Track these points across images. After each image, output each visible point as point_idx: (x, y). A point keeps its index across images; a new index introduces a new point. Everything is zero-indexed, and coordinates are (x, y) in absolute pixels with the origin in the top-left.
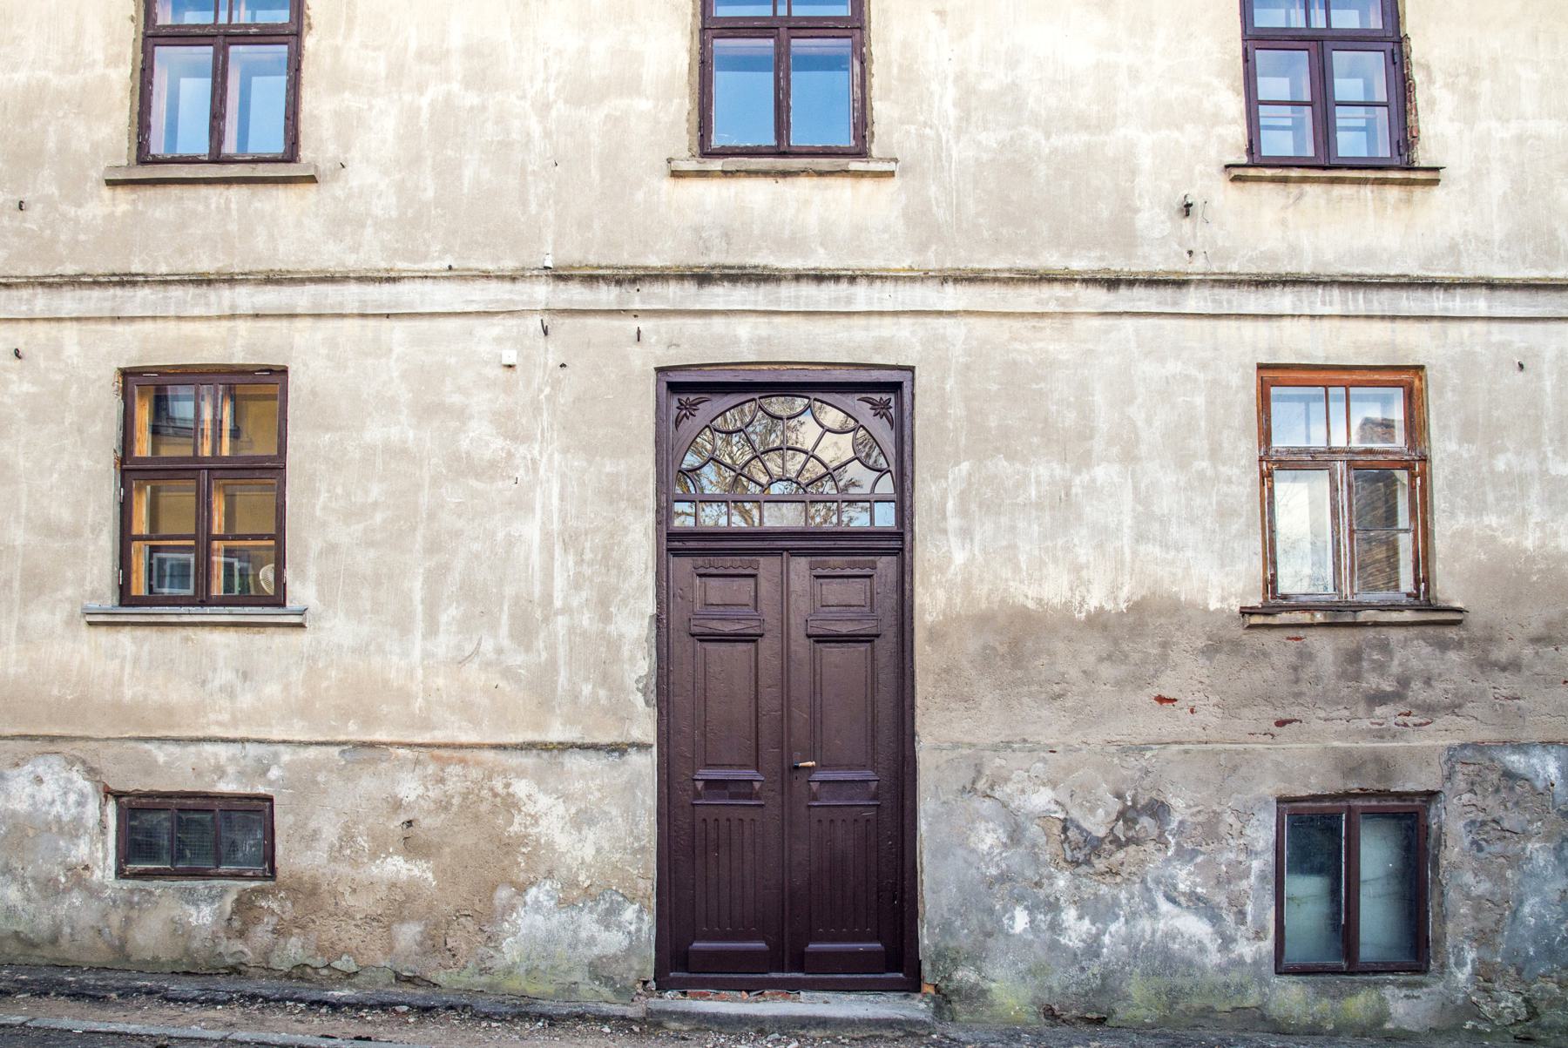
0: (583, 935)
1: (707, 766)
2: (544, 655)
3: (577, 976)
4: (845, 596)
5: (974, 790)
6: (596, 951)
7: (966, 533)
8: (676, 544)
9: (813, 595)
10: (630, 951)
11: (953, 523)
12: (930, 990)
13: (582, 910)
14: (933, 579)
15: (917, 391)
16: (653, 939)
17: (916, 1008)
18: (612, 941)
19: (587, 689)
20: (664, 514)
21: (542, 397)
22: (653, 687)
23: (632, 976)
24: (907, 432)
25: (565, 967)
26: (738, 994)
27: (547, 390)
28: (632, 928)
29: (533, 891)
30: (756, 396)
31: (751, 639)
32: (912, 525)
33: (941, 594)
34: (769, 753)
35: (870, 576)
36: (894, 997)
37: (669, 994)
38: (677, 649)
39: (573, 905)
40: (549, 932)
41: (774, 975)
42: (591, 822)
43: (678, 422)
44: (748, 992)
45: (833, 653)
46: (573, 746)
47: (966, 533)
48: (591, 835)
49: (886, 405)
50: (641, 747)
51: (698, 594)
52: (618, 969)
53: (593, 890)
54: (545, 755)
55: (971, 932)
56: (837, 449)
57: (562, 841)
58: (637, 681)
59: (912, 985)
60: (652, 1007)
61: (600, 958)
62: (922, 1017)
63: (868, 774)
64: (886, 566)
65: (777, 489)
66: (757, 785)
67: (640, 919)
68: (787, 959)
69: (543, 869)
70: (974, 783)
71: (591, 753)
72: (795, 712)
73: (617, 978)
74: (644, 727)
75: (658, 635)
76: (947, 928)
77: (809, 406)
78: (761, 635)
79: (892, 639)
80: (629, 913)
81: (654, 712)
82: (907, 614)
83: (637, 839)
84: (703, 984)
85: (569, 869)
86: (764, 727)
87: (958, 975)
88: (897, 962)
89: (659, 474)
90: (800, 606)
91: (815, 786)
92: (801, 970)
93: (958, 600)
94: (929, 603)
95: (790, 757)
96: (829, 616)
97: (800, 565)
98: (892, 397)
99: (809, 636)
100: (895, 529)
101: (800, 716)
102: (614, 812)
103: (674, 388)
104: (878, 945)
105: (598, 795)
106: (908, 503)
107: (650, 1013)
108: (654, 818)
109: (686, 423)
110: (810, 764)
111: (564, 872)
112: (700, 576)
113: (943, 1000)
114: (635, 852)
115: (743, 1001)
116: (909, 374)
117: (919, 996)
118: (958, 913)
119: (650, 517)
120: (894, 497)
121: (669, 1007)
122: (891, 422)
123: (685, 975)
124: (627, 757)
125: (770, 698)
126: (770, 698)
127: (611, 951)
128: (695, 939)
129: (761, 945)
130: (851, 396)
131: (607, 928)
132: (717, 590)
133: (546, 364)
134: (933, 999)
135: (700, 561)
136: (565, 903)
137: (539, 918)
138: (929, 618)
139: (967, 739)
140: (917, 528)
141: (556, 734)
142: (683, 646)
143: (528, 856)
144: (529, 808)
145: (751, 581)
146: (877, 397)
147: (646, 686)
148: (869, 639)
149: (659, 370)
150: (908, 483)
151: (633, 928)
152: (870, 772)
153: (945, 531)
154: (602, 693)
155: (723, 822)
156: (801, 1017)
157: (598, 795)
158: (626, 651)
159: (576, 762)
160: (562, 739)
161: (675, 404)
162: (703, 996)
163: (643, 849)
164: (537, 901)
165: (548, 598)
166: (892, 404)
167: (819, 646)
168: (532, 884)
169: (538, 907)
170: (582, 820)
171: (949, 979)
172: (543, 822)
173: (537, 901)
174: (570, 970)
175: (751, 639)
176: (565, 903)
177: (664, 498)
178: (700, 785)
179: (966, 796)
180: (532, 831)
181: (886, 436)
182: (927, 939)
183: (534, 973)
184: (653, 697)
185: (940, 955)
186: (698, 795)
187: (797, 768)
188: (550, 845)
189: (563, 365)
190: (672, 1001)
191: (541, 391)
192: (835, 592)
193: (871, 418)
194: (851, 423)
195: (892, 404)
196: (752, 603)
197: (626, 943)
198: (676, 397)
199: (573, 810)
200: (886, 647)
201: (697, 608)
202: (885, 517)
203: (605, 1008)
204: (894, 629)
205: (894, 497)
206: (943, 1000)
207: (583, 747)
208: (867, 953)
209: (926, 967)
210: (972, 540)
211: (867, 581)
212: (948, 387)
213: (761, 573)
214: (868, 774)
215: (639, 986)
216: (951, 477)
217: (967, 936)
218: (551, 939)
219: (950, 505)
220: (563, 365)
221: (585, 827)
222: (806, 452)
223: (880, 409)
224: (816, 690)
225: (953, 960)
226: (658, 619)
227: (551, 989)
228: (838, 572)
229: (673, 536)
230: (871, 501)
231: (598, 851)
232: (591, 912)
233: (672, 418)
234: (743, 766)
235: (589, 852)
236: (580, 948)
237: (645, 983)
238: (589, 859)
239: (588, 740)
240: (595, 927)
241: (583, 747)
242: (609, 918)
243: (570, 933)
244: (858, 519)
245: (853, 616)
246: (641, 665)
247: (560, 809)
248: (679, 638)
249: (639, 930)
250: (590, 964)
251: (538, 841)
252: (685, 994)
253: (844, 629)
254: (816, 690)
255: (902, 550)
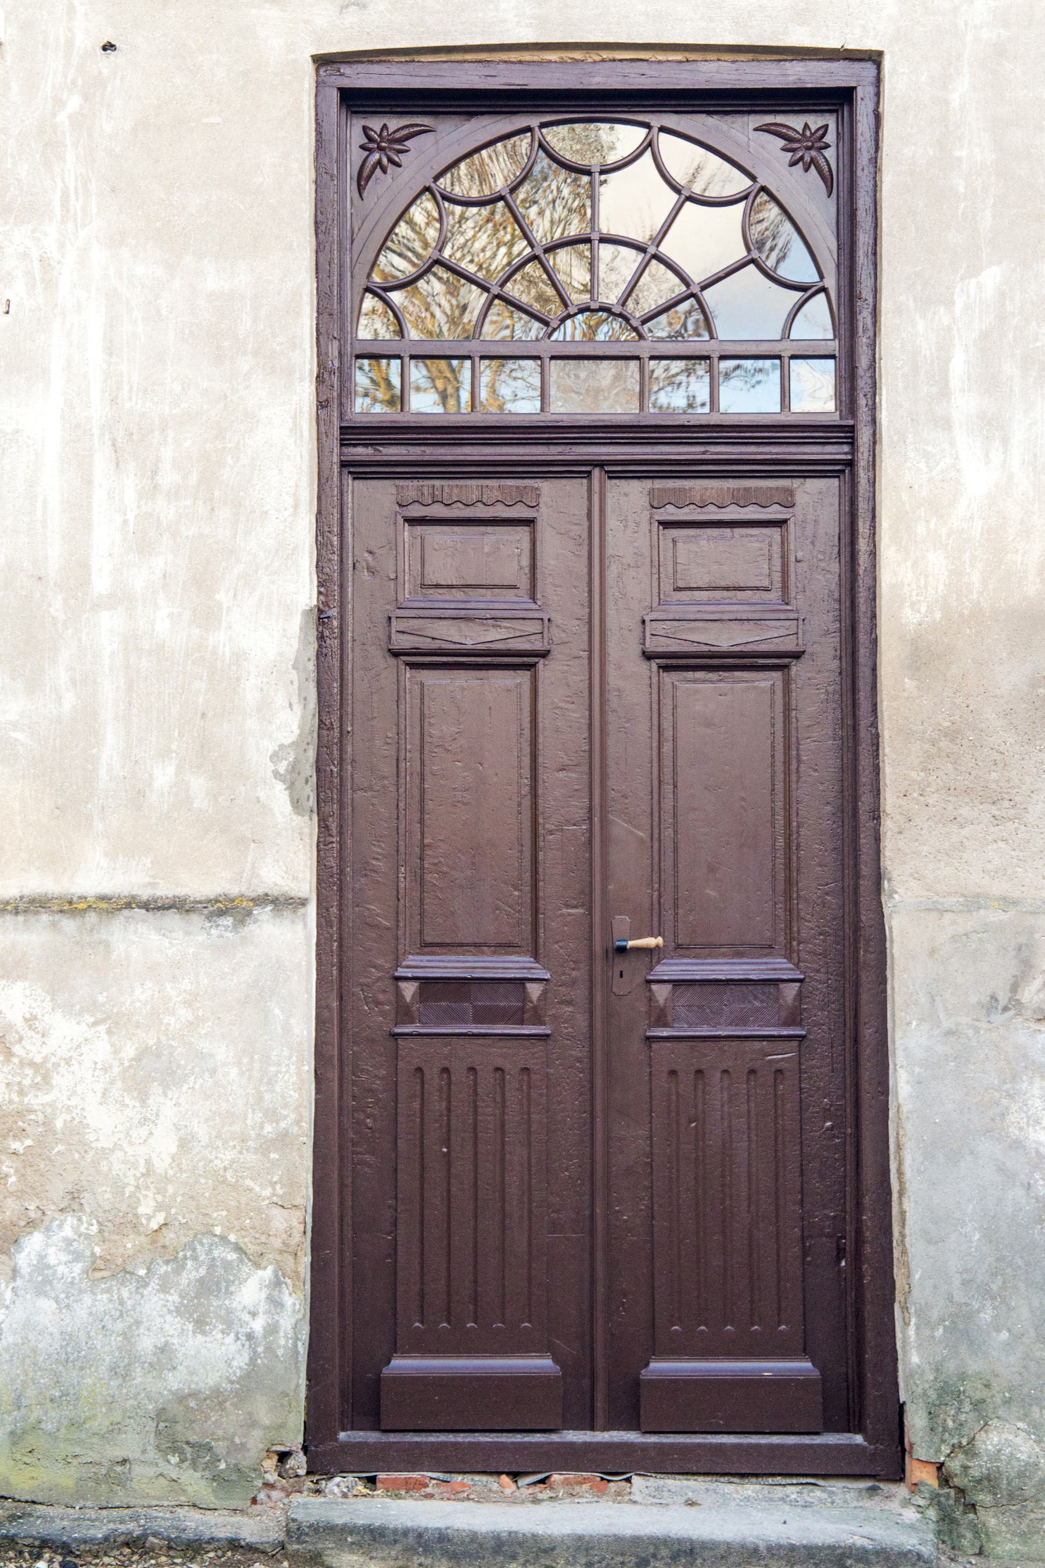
0: (146, 1343)
1: (427, 947)
2: (69, 700)
3: (129, 1445)
4: (724, 570)
5: (1013, 1005)
6: (174, 1381)
7: (992, 427)
8: (362, 451)
9: (657, 567)
10: (250, 1382)
11: (964, 404)
12: (928, 1478)
13: (143, 1283)
14: (921, 529)
15: (888, 108)
16: (303, 1349)
17: (896, 1518)
18: (211, 1357)
19: (163, 775)
20: (332, 384)
21: (62, 117)
22: (309, 770)
23: (255, 1442)
24: (863, 201)
25: (100, 1422)
26: (491, 1481)
27: (74, 103)
28: (260, 1319)
29: (34, 1242)
30: (534, 121)
31: (525, 661)
32: (873, 408)
33: (937, 563)
34: (562, 916)
35: (781, 523)
36: (843, 1492)
37: (336, 1485)
38: (359, 684)
39: (124, 1273)
40: (68, 1337)
41: (573, 1436)
42: (170, 1078)
43: (362, 180)
44: (515, 1475)
45: (701, 694)
46: (130, 903)
47: (992, 427)
48: (167, 1107)
49: (817, 141)
50: (283, 904)
51: (409, 564)
52: (222, 1426)
53: (169, 1237)
54: (69, 925)
55: (1017, 1337)
56: (707, 240)
57: (103, 1123)
58: (275, 757)
59: (885, 1461)
60: (300, 1515)
61: (181, 1398)
62: (910, 1542)
63: (777, 966)
64: (816, 500)
65: (573, 330)
66: (534, 990)
67: (275, 1303)
68: (605, 1404)
69: (57, 1190)
70: (1015, 988)
71: (172, 919)
72: (619, 827)
73: (220, 1447)
74: (288, 857)
75: (321, 655)
76: (961, 1328)
77: (649, 145)
78: (544, 654)
79: (837, 659)
80: (251, 1290)
81: (308, 827)
82: (863, 606)
83: (272, 1116)
84: (414, 1459)
85: (119, 1189)
86: (551, 753)
87: (991, 1441)
88: (848, 1409)
89: (323, 296)
90: (630, 590)
91: (661, 993)
92: (634, 1424)
93: (975, 578)
94: (913, 580)
95: (608, 927)
96: (691, 612)
97: (629, 498)
98: (830, 120)
99: (648, 656)
100: (835, 419)
101: (628, 833)
102: (222, 1053)
103: (355, 101)
104: (803, 1366)
105: (185, 1014)
106: (863, 362)
107: (295, 1531)
108: (309, 1066)
109: (381, 184)
110: (651, 942)
111: (105, 1195)
112: (412, 521)
113: (958, 1501)
114: (265, 1147)
115: (503, 1499)
116: (869, 69)
117: (901, 1490)
118: (987, 1294)
119: (306, 393)
120: (834, 347)
121: (339, 1516)
122: (828, 180)
123: (373, 1437)
124: (251, 928)
125: (563, 792)
126: (563, 792)
127: (209, 1380)
128: (395, 1349)
129: (542, 1364)
130: (740, 120)
131: (201, 1325)
132: (449, 554)
133: (70, 43)
134: (935, 1499)
135: (411, 488)
136: (107, 1269)
137: (47, 1305)
138: (910, 617)
139: (999, 887)
140: (884, 416)
141: (93, 878)
142: (373, 675)
143: (26, 1161)
144: (30, 1048)
145: (522, 533)
146: (796, 122)
147: (294, 768)
148: (779, 661)
149: (322, 61)
150: (864, 317)
151: (258, 1325)
152: (782, 962)
153: (945, 423)
154: (198, 784)
155: (459, 1074)
156: (636, 1541)
157: (185, 1014)
158: (250, 692)
159: (137, 940)
160: (107, 887)
161: (357, 137)
162: (413, 1487)
163: (283, 1139)
164: (42, 1265)
165: (78, 572)
166: (830, 138)
167: (669, 678)
168: (32, 1225)
169: (43, 1280)
170: (149, 1073)
171: (969, 1449)
172: (61, 1080)
173: (42, 1265)
174: (116, 1429)
175: (525, 661)
176: (107, 1269)
177: (333, 349)
178: (409, 990)
179: (998, 1018)
180: (36, 1100)
181: (817, 209)
182: (918, 1353)
183: (31, 1441)
184: (309, 793)
185: (947, 1392)
186: (404, 1013)
187: (622, 950)
188: (76, 1132)
189: (108, 47)
190: (344, 1501)
191: (59, 103)
192: (704, 556)
193: (784, 169)
194: (742, 183)
195: (830, 138)
196: (524, 583)
197: (241, 1361)
198: (358, 124)
199: (129, 1051)
200: (816, 679)
201: (406, 594)
202: (815, 393)
203: (194, 1523)
204: (834, 640)
205: (834, 347)
206: (958, 1501)
207: (152, 906)
208: (781, 1384)
209: (916, 1421)
210: (1005, 441)
211: (775, 533)
212: (955, 98)
213: (544, 516)
214: (777, 966)
215: (270, 1463)
216: (959, 301)
217: (1009, 1347)
218: (73, 1354)
219: (958, 367)
220: (108, 47)
221: (156, 1088)
222: (641, 248)
223: (803, 151)
224: (663, 778)
225: (978, 1405)
226: (321, 617)
227: (66, 1478)
228: (712, 514)
229: (352, 434)
230: (780, 356)
231: (185, 1144)
232: (164, 1288)
233: (351, 170)
234: (506, 947)
235: (162, 1147)
236: (138, 1377)
237: (283, 1457)
238: (161, 1165)
239: (165, 890)
240: (173, 1325)
241: (152, 906)
242: (203, 1305)
243: (116, 1341)
244: (749, 398)
245: (743, 611)
246: (280, 719)
247: (101, 1049)
248: (371, 662)
249: (272, 1329)
250: (161, 1414)
251: (48, 1124)
252: (372, 1481)
253: (726, 639)
254: (663, 778)
255: (851, 464)
